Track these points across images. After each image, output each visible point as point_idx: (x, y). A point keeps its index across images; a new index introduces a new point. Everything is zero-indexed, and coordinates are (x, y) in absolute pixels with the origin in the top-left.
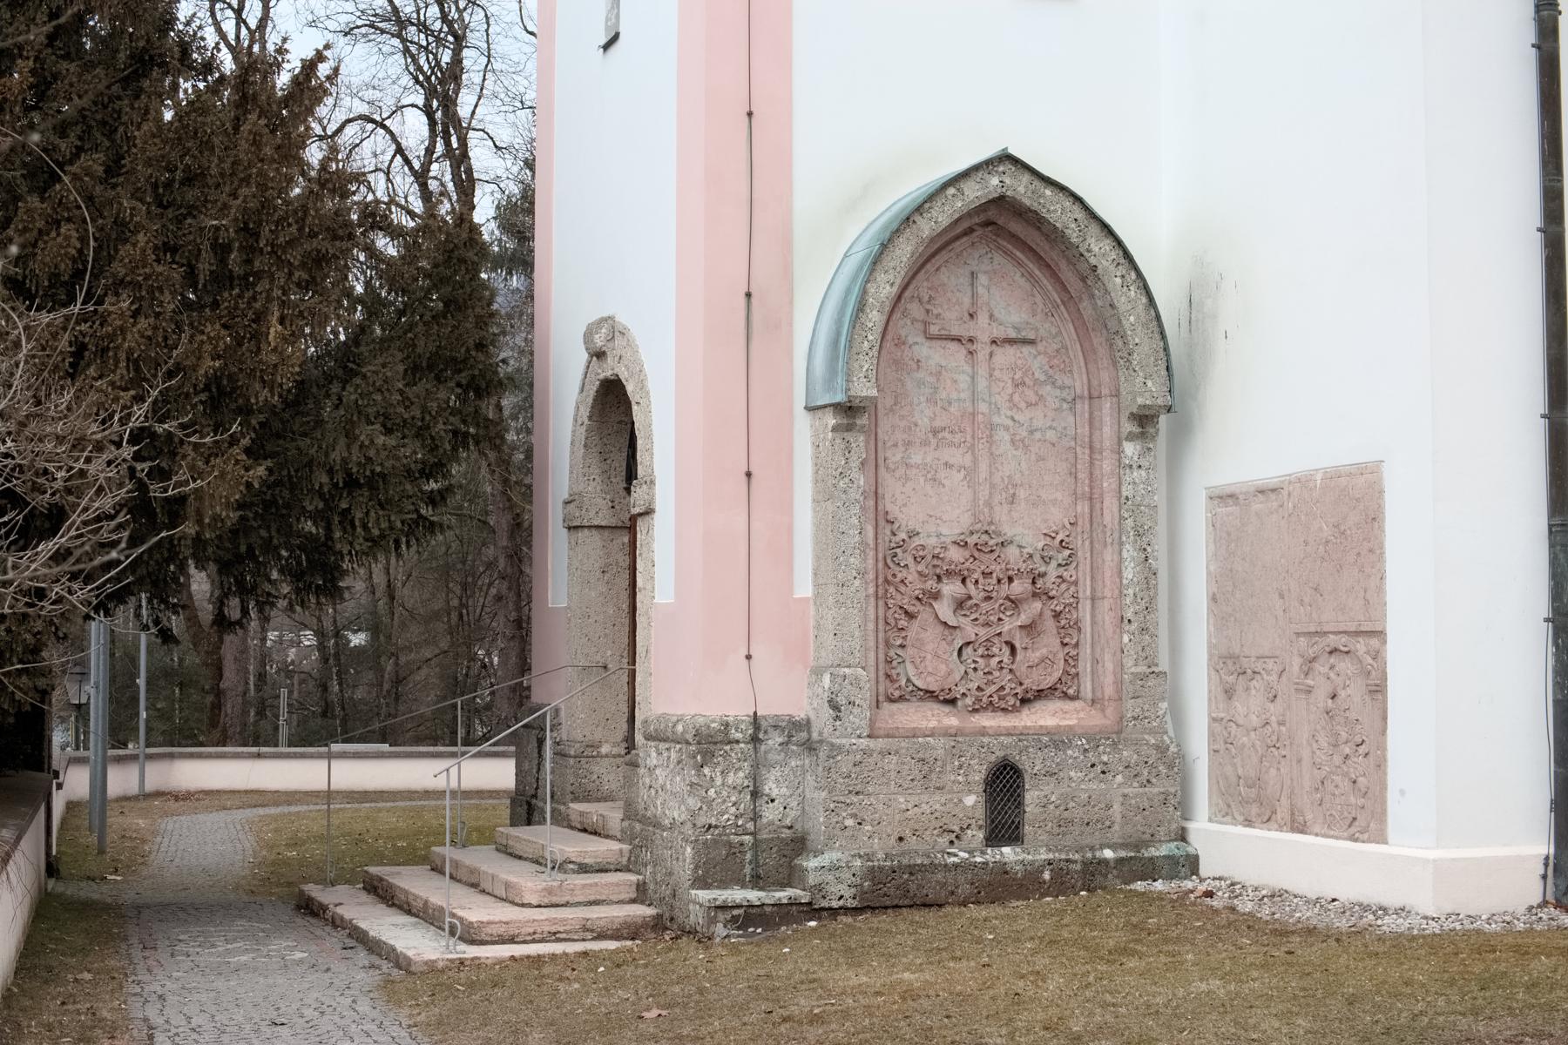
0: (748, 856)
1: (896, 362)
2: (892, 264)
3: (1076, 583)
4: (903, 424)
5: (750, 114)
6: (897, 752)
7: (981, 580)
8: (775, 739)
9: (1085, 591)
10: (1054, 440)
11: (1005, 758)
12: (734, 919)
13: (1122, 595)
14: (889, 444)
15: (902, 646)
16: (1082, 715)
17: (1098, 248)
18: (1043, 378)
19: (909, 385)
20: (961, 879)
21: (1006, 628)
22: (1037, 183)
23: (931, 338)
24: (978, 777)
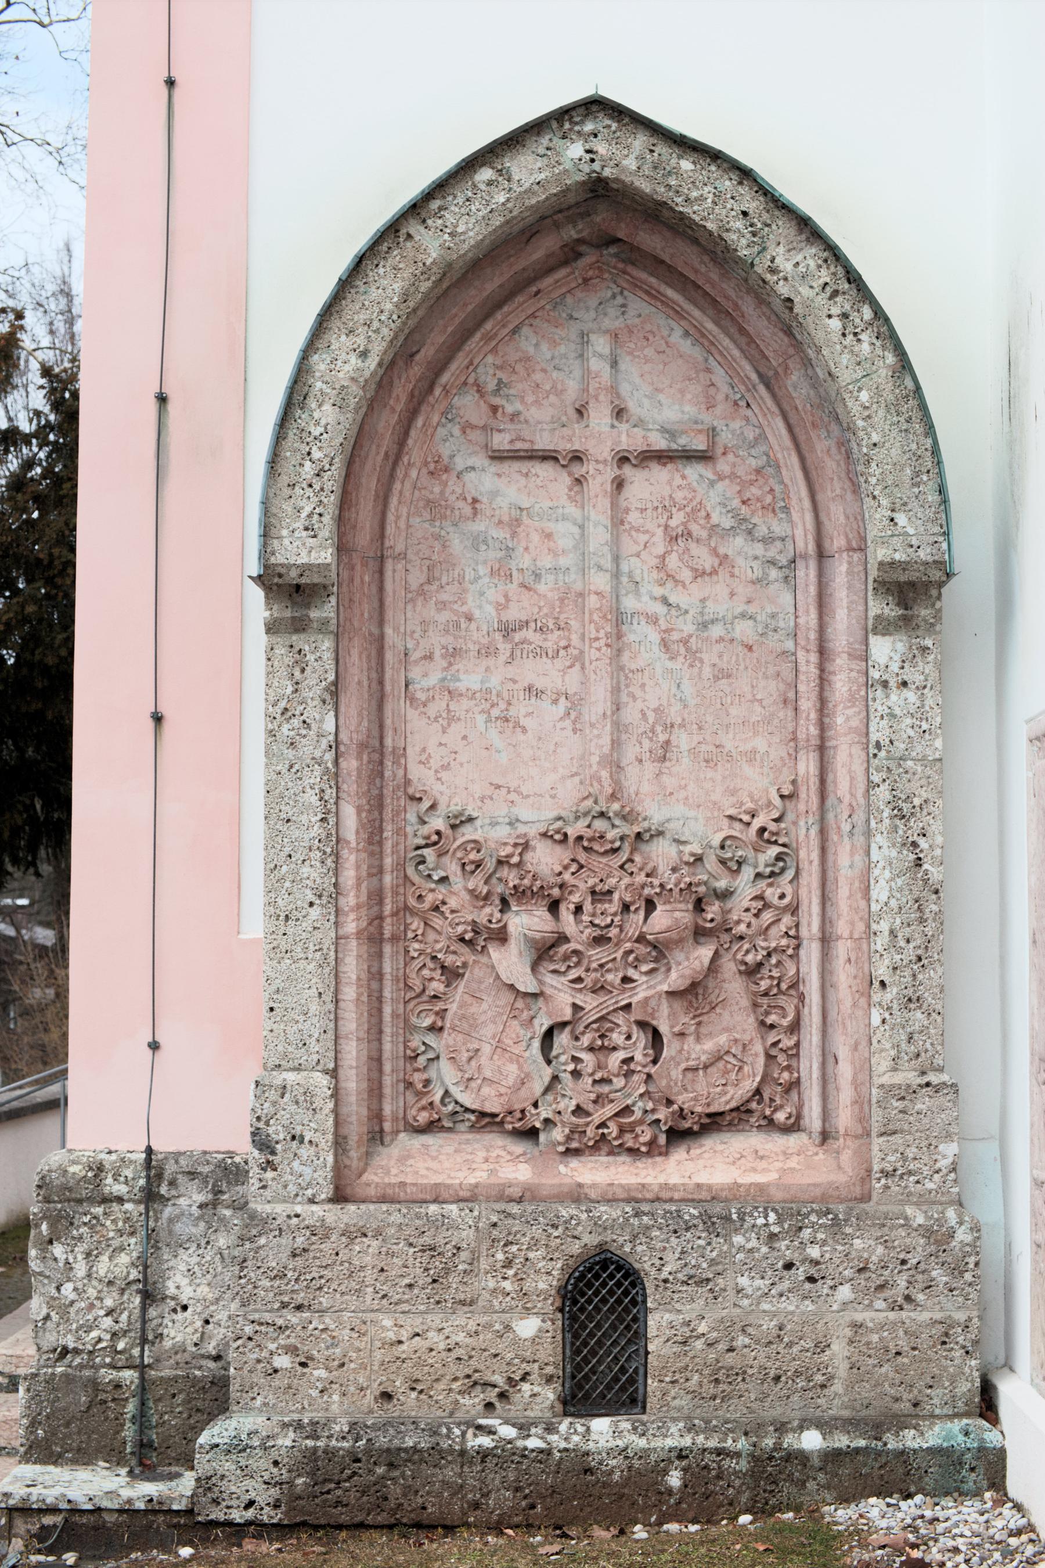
0: (131, 1408)
1: (430, 504)
2: (362, 317)
3: (794, 909)
4: (444, 617)
5: (171, 83)
6: (378, 1233)
7: (588, 907)
8: (191, 1197)
9: (811, 926)
10: (751, 637)
11: (602, 1248)
12: (44, 1532)
13: (870, 934)
14: (415, 656)
15: (434, 1029)
16: (793, 1163)
17: (792, 266)
18: (727, 522)
19: (456, 544)
20: (495, 1480)
21: (641, 994)
22: (663, 149)
23: (498, 457)
24: (546, 1280)
